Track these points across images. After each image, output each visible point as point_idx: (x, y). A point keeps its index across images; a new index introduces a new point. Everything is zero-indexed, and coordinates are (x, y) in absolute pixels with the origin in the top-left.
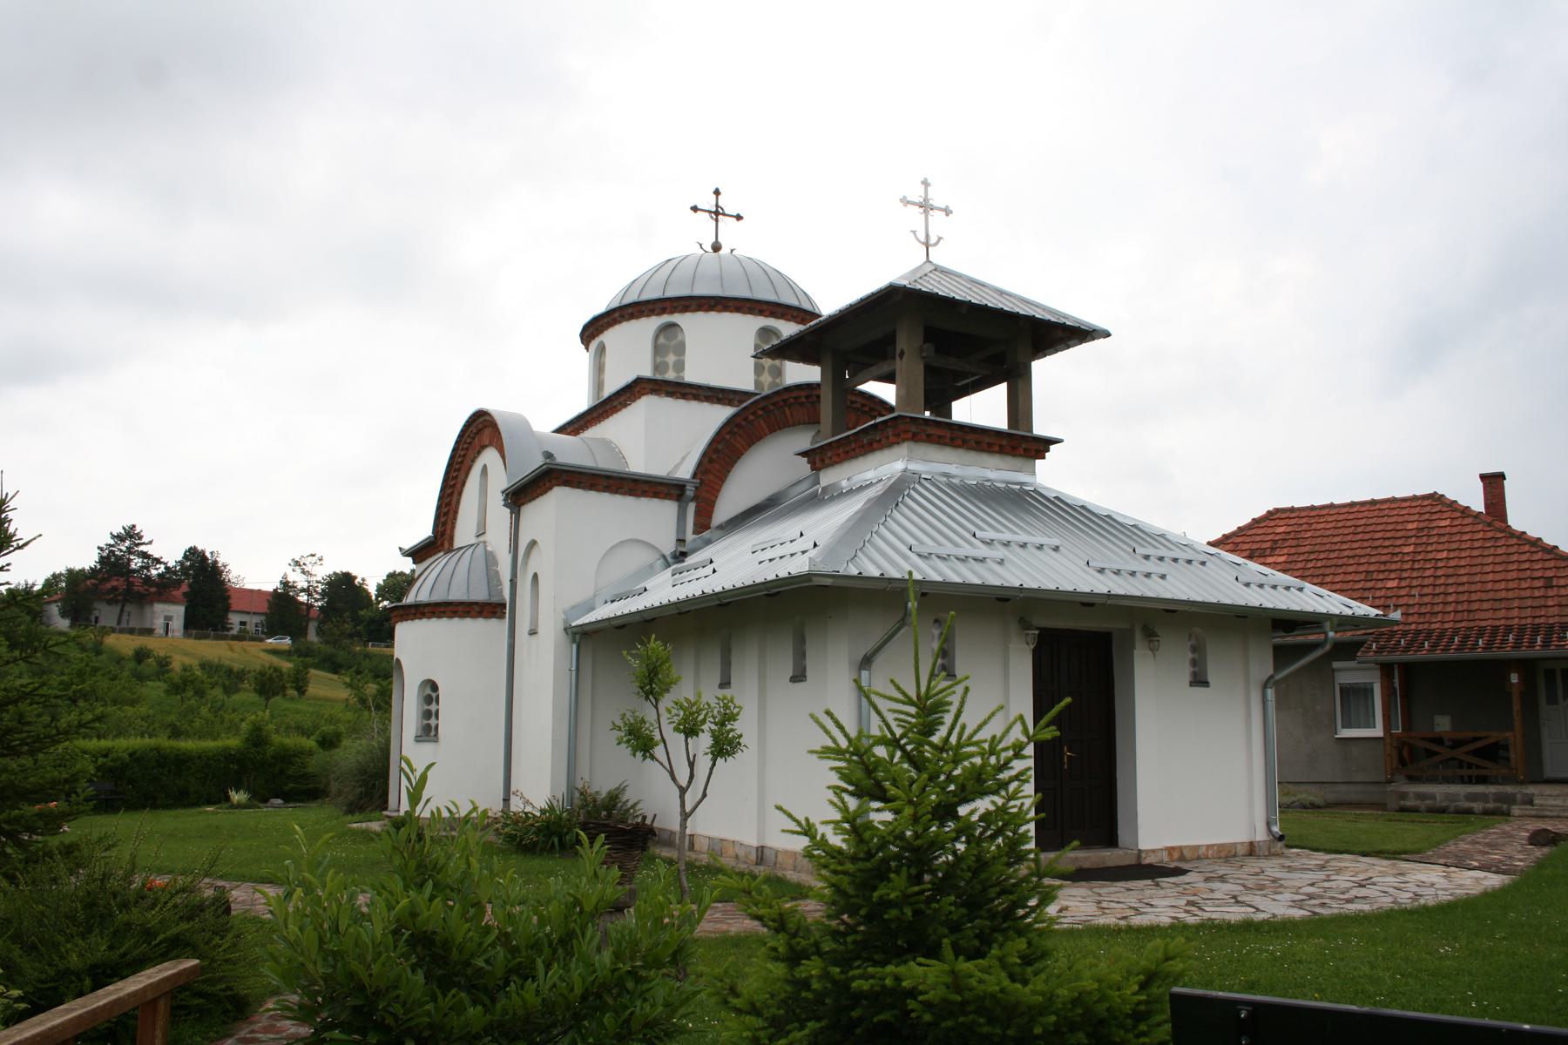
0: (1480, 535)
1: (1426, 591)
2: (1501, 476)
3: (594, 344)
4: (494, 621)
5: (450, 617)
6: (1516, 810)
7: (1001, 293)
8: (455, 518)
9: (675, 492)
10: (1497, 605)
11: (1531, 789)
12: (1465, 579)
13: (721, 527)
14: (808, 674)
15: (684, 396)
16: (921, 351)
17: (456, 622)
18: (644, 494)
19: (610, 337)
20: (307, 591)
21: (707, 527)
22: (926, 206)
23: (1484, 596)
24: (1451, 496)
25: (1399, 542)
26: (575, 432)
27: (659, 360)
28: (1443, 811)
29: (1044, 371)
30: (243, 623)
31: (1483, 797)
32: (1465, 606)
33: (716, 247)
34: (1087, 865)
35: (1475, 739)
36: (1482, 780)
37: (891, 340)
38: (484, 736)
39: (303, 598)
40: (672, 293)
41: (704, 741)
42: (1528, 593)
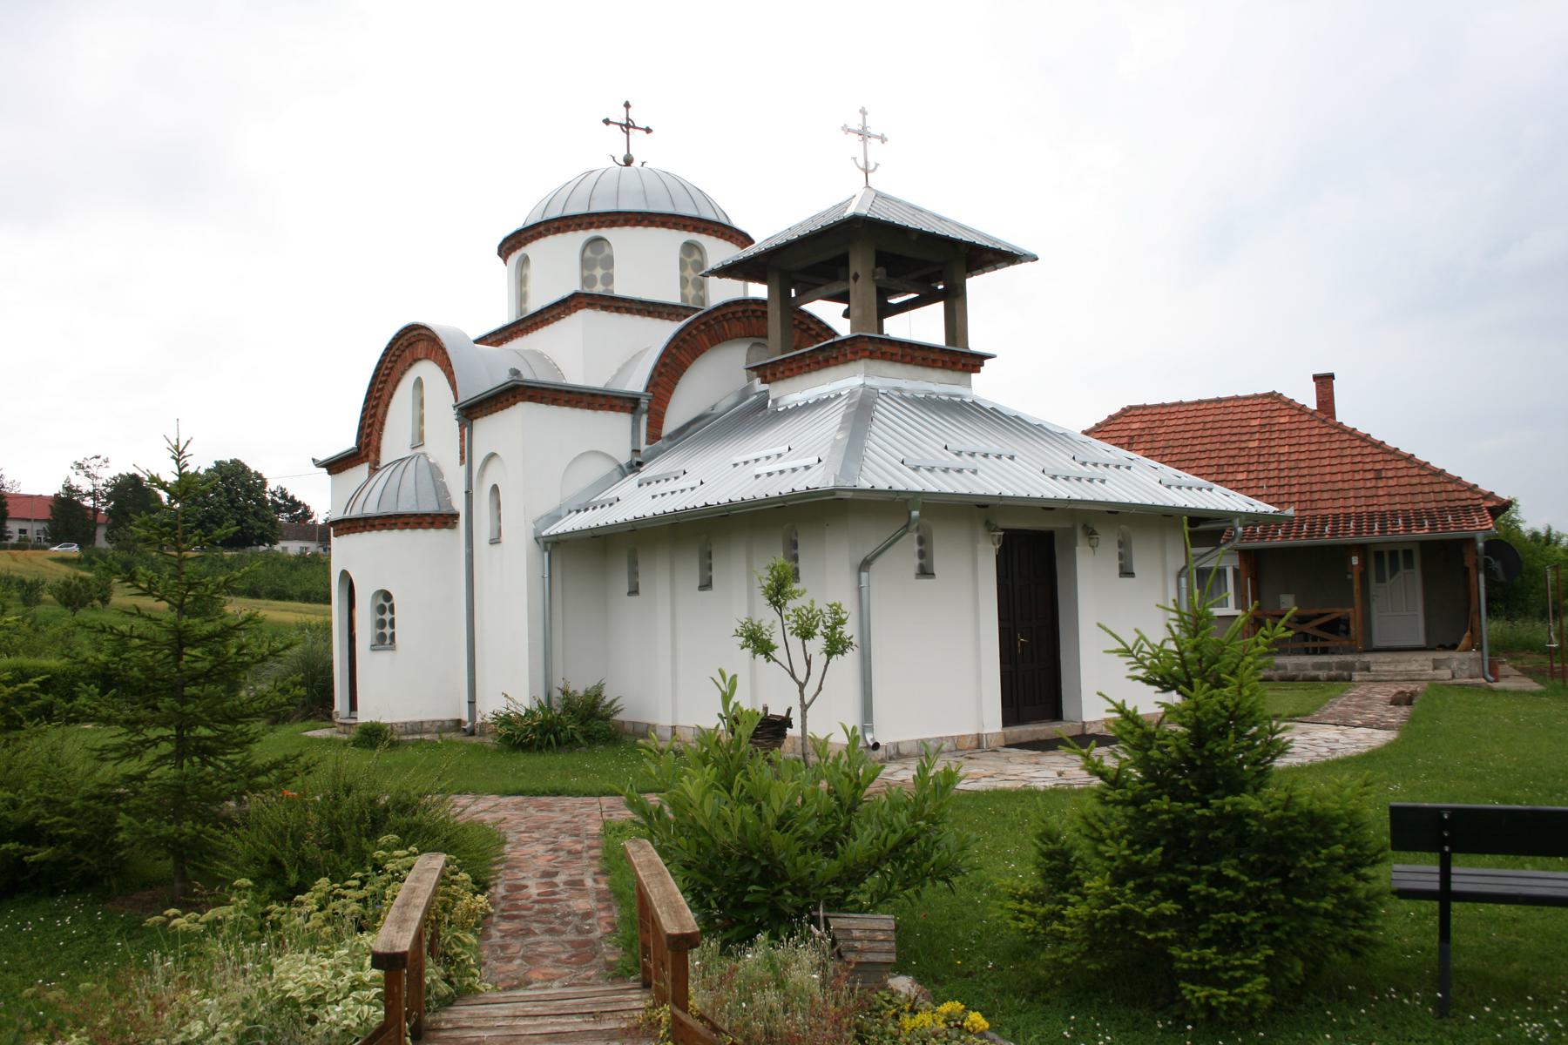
0: (1316, 431)
1: (1272, 482)
2: (1331, 376)
3: (514, 257)
4: (445, 531)
5: (401, 528)
6: (1356, 676)
7: (940, 219)
8: (381, 429)
9: (629, 405)
10: (1335, 495)
11: (1368, 658)
12: (1305, 472)
13: (670, 437)
14: (801, 575)
15: (618, 310)
16: (874, 274)
17: (408, 534)
18: (601, 407)
19: (533, 249)
20: (93, 495)
21: (658, 437)
22: (864, 134)
23: (1324, 487)
24: (1288, 395)
25: (1245, 438)
26: (498, 343)
27: (586, 273)
28: (1293, 679)
29: (977, 286)
30: (22, 531)
31: (1328, 666)
32: (1308, 496)
33: (628, 161)
34: (1043, 737)
35: (1321, 615)
36: (1325, 651)
37: (843, 261)
38: (437, 643)
39: (89, 502)
40: (597, 207)
41: (817, 644)
42: (1361, 484)
